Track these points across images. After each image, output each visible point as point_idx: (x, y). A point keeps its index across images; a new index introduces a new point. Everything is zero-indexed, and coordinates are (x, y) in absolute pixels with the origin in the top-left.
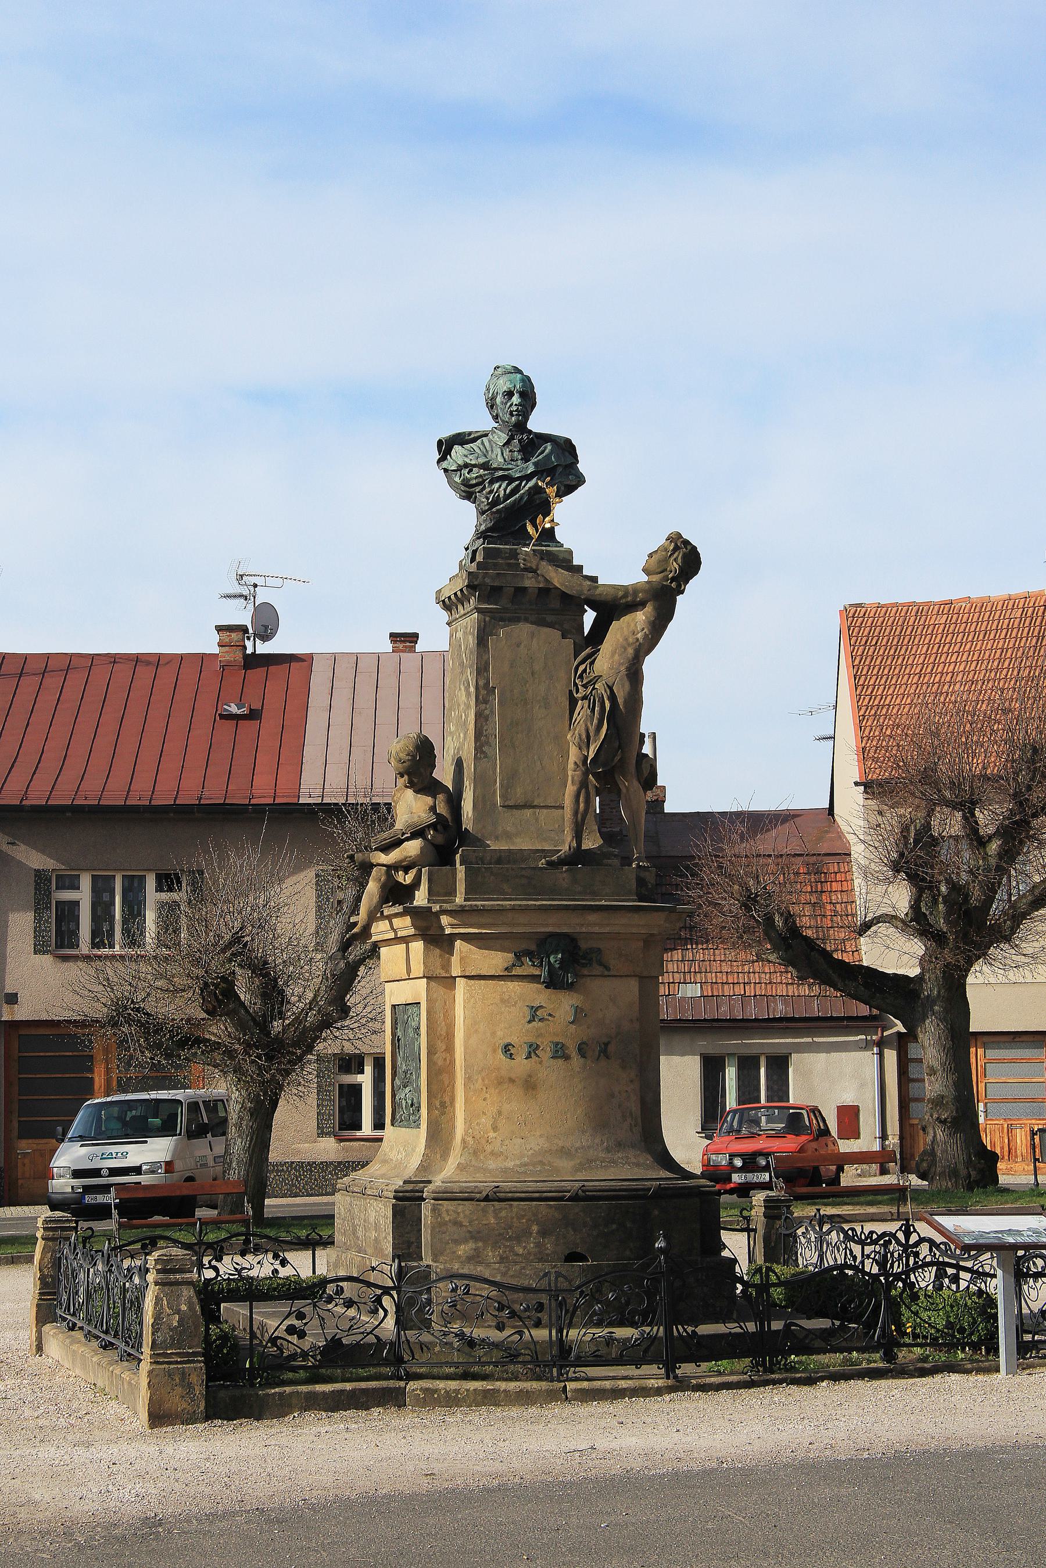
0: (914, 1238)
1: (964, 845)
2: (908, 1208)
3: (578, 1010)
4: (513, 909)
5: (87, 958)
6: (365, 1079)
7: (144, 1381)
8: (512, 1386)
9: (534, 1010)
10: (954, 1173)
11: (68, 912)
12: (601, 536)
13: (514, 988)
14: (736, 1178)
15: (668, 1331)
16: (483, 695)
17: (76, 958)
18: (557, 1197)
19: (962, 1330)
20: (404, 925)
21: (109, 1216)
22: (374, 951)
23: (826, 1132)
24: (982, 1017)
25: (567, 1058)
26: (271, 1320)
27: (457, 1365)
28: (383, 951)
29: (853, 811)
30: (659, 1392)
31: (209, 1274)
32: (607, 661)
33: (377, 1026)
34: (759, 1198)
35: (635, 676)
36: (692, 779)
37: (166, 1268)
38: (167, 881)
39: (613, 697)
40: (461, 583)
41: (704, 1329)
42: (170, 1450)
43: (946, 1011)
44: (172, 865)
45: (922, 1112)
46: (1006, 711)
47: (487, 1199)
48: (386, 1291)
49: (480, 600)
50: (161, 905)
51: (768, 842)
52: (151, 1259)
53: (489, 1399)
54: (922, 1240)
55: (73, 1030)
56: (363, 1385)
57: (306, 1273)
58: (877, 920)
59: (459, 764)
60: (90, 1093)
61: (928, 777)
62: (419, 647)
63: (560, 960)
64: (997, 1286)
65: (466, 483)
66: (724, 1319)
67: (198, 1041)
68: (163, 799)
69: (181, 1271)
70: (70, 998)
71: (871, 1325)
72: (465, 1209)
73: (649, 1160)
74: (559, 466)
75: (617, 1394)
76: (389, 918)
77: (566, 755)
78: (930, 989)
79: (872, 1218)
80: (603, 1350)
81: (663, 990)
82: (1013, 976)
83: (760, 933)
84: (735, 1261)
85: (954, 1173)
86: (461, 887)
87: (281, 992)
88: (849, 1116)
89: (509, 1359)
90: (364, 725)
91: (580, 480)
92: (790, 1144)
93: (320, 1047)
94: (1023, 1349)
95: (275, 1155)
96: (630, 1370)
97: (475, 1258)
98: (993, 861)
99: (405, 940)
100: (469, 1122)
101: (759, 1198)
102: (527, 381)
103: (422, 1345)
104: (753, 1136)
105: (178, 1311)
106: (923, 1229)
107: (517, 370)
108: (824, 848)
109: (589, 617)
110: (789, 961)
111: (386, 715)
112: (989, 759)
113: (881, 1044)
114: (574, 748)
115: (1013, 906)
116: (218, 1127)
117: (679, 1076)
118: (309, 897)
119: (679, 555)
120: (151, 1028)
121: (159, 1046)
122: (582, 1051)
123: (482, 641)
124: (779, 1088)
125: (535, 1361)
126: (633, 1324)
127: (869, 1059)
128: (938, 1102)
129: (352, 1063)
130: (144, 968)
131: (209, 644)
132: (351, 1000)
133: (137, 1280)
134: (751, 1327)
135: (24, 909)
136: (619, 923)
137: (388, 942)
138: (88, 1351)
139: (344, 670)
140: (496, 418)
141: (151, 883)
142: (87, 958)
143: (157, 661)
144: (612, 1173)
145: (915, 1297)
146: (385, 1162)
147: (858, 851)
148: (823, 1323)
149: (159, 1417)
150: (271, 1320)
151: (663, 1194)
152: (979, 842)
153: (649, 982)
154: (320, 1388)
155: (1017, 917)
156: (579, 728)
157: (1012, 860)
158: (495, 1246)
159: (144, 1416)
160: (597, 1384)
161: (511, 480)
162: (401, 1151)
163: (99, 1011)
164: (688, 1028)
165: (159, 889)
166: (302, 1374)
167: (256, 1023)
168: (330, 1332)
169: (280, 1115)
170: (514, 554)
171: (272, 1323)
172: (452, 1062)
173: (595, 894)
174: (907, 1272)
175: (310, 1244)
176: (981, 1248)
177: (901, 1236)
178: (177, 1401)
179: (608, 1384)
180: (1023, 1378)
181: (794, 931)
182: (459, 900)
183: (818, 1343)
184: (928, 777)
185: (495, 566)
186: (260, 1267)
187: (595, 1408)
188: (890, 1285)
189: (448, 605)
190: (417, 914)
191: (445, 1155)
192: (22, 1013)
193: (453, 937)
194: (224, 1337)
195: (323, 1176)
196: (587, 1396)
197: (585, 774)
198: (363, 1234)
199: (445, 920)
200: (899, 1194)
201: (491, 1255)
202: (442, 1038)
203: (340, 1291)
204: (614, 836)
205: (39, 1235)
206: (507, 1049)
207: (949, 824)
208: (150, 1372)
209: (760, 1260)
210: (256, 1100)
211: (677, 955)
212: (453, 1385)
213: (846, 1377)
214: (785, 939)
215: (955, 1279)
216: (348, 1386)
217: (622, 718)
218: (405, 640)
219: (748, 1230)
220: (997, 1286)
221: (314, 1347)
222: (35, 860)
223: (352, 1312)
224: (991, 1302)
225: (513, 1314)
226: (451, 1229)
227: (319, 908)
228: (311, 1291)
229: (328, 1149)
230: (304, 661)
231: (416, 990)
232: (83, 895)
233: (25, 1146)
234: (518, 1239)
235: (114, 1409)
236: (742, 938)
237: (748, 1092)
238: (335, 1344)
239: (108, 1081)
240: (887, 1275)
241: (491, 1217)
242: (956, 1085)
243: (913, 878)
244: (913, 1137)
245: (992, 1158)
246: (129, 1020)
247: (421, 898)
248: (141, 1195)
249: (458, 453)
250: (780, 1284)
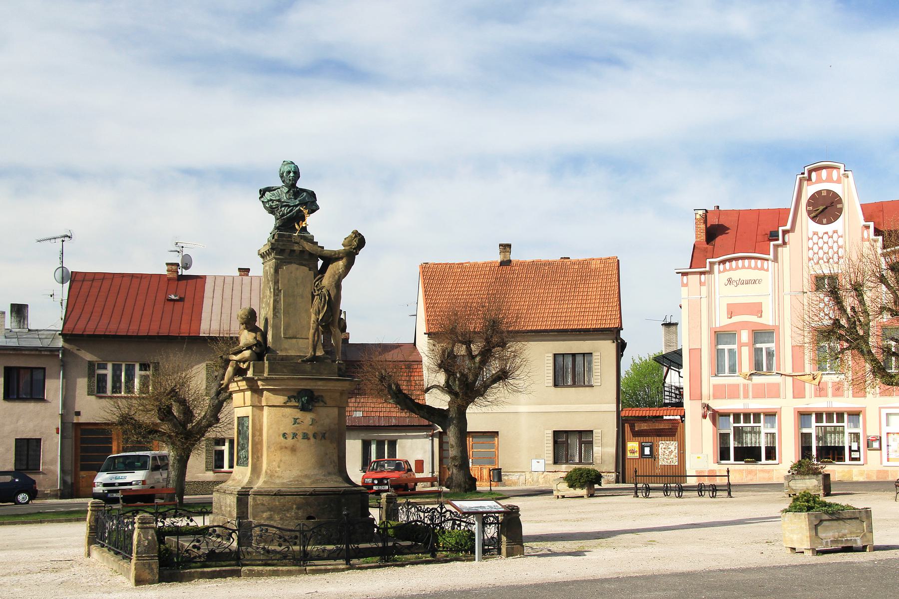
0: (444, 510)
1: (467, 358)
2: (442, 499)
3: (313, 420)
4: (288, 379)
5: (111, 397)
6: (226, 448)
7: (133, 567)
8: (285, 568)
9: (295, 420)
10: (459, 486)
11: (102, 379)
12: (325, 229)
13: (288, 411)
14: (375, 488)
15: (347, 547)
16: (277, 292)
17: (105, 397)
18: (304, 494)
19: (461, 545)
20: (243, 385)
21: (118, 502)
22: (230, 397)
23: (410, 470)
24: (472, 425)
25: (309, 439)
26: (186, 543)
27: (262, 560)
28: (234, 395)
29: (424, 345)
30: (343, 570)
31: (160, 524)
32: (327, 280)
33: (230, 426)
34: (384, 495)
35: (338, 287)
36: (360, 331)
37: (143, 522)
38: (144, 367)
39: (329, 295)
40: (267, 248)
41: (361, 546)
42: (143, 594)
43: (458, 423)
44: (146, 360)
45: (449, 462)
46: (483, 307)
47: (275, 495)
48: (234, 531)
49: (276, 254)
50: (141, 376)
51: (389, 356)
52: (136, 519)
53: (276, 574)
54: (447, 511)
55: (107, 427)
56: (224, 568)
57: (200, 525)
58: (433, 387)
59: (266, 320)
60: (111, 453)
61: (453, 331)
62: (250, 274)
63: (306, 400)
64: (475, 528)
65: (271, 207)
66: (370, 541)
67: (157, 431)
68: (143, 333)
69: (149, 523)
70: (103, 414)
71: (426, 544)
72: (267, 498)
73: (341, 479)
74: (310, 202)
75: (327, 571)
76: (237, 382)
77: (310, 317)
78: (452, 414)
79: (428, 503)
80: (322, 554)
81: (347, 414)
82: (484, 409)
83: (386, 392)
84: (374, 519)
85: (459, 486)
86: (266, 370)
87: (191, 412)
88: (420, 464)
89: (284, 559)
90: (227, 305)
91: (318, 208)
92: (396, 475)
93: (207, 434)
94: (484, 552)
95: (188, 478)
96: (332, 562)
97: (270, 518)
98: (477, 365)
99: (243, 391)
100: (268, 464)
101: (384, 495)
102: (296, 167)
103: (248, 553)
104: (382, 471)
105: (147, 539)
106: (448, 507)
107: (292, 163)
108: (411, 358)
109: (320, 263)
110: (397, 403)
111: (236, 301)
112: (476, 325)
113: (433, 436)
114: (312, 316)
115: (485, 382)
116: (165, 467)
117: (353, 448)
118: (203, 375)
119: (357, 239)
120: (138, 426)
121: (140, 433)
122: (315, 436)
123: (276, 271)
124: (392, 453)
125: (294, 558)
126: (334, 544)
127: (428, 442)
128: (454, 458)
129: (220, 442)
130: (134, 401)
131: (164, 270)
132: (220, 416)
133: (130, 527)
134: (380, 545)
135: (84, 377)
136: (330, 385)
137: (236, 392)
138: (110, 556)
139: (219, 282)
140: (283, 182)
141: (137, 367)
142: (111, 397)
143: (142, 276)
144: (326, 485)
145: (444, 532)
146: (234, 480)
147: (425, 360)
148: (408, 543)
149: (139, 581)
150: (186, 543)
151: (346, 493)
152: (473, 357)
153: (342, 409)
154: (206, 570)
155: (486, 386)
156: (315, 307)
157: (485, 365)
158: (278, 513)
159: (133, 581)
160: (319, 567)
161: (289, 206)
162: (241, 476)
163: (115, 419)
164: (357, 429)
165: (141, 370)
166: (199, 564)
167: (181, 425)
168: (211, 547)
169: (190, 462)
170: (290, 236)
171: (186, 544)
172: (262, 440)
173: (321, 374)
174: (441, 522)
175: (203, 513)
176: (470, 513)
177: (439, 509)
178: (147, 575)
179: (323, 567)
180: (484, 562)
181: (399, 391)
182: (266, 375)
183: (406, 551)
184: (453, 331)
185: (282, 241)
186: (182, 522)
187: (318, 576)
188: (434, 528)
189: (263, 256)
190: (248, 380)
191: (258, 477)
192: (82, 419)
193: (263, 390)
194: (167, 550)
195: (207, 487)
196: (314, 572)
197: (318, 326)
198: (225, 506)
199: (259, 383)
200: (438, 494)
201: (277, 517)
202: (258, 430)
203: (215, 531)
204: (330, 352)
205: (89, 509)
206: (284, 435)
207: (461, 350)
208: (136, 564)
209: (384, 519)
210: (181, 456)
211: (353, 400)
212: (260, 568)
213: (417, 563)
214: (396, 394)
215: (459, 525)
216: (218, 569)
217: (333, 304)
218: (245, 271)
219: (379, 507)
220: (475, 528)
221: (204, 553)
222: (88, 357)
223: (219, 540)
224: (473, 534)
225: (285, 540)
226: (261, 507)
227: (207, 378)
228: (203, 531)
229: (210, 476)
230: (203, 278)
231: (247, 411)
232: (109, 372)
233: (83, 474)
234: (288, 510)
235: (121, 578)
236: (379, 394)
237: (380, 454)
238: (212, 552)
239: (118, 446)
240: (433, 524)
241: (277, 502)
242: (461, 452)
243: (446, 371)
244: (444, 473)
245: (475, 480)
246: (127, 423)
247: (250, 374)
248: (132, 494)
249: (268, 195)
250: (392, 528)
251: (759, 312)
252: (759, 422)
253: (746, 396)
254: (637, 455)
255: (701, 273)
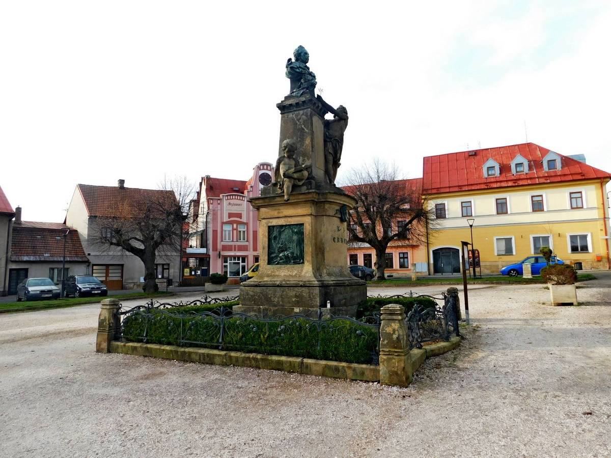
4: (488, 288)
251: (241, 217)
252: (239, 260)
253: (235, 250)
254: (188, 274)
255: (218, 199)
